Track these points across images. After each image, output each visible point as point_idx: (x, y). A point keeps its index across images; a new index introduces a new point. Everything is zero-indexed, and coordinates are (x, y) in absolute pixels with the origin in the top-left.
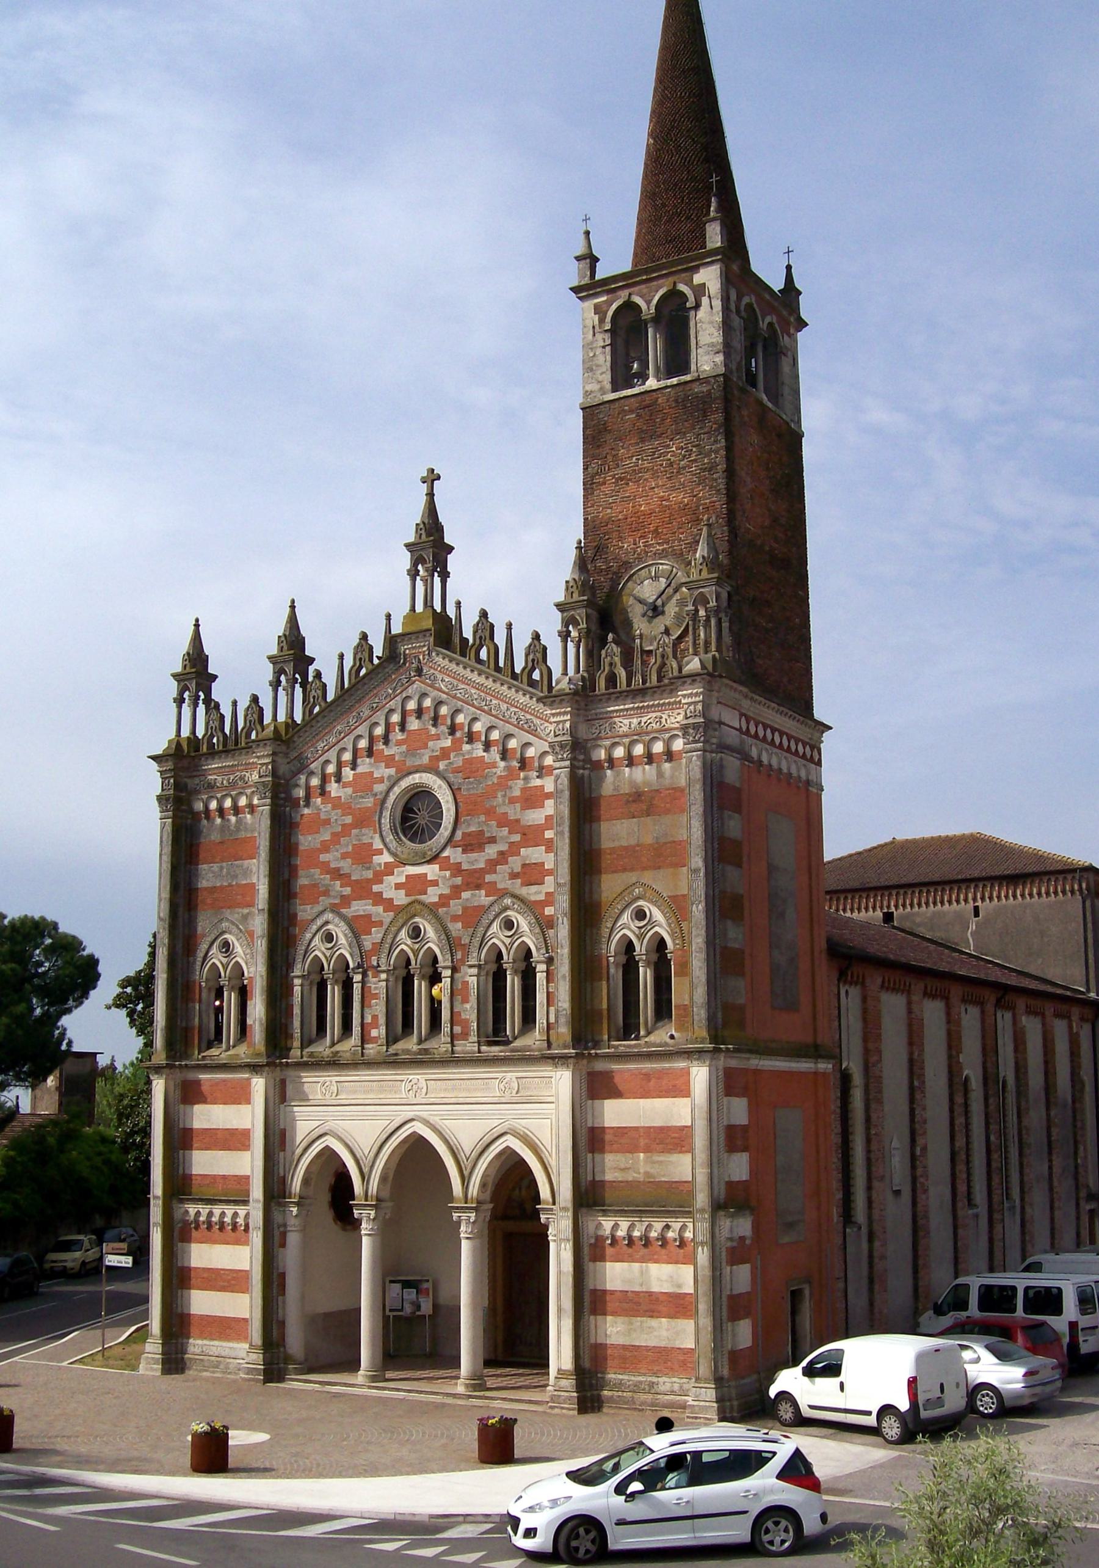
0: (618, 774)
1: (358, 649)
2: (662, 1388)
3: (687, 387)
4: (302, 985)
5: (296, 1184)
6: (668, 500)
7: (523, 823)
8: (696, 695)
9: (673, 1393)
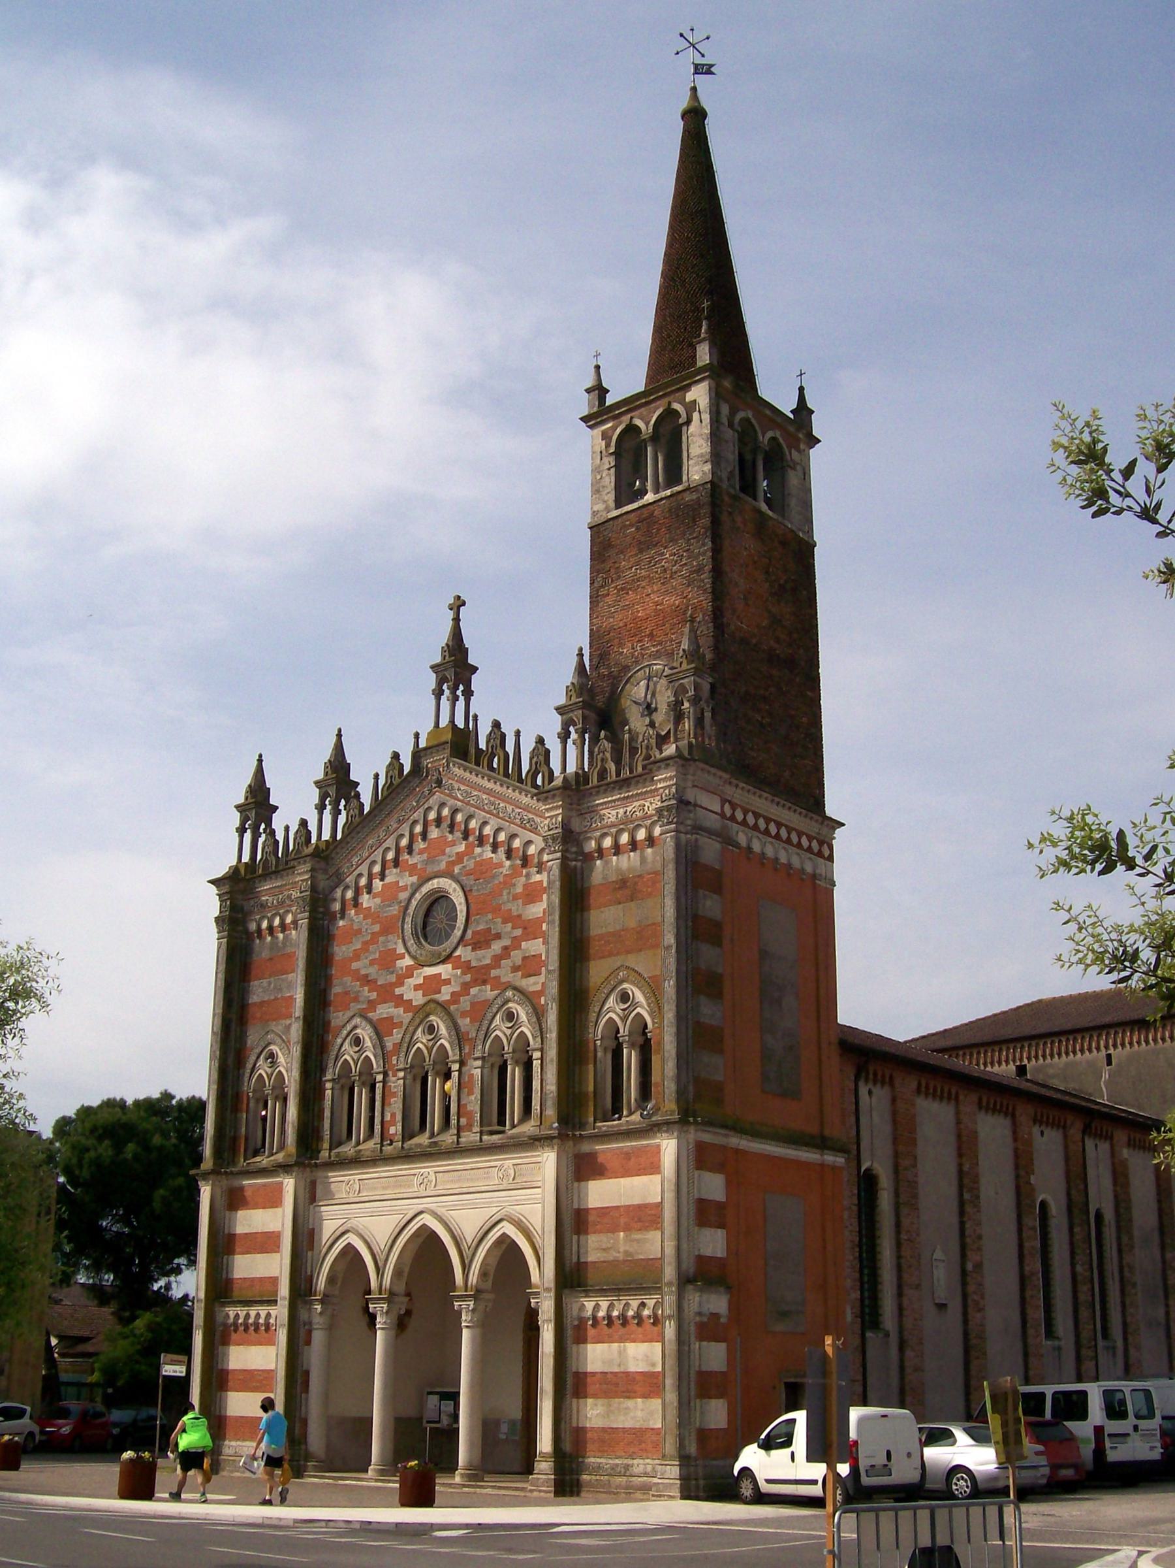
0: (607, 863)
1: (390, 767)
2: (636, 1470)
3: (680, 497)
4: (332, 1089)
5: (321, 1282)
7: (524, 917)
8: (671, 778)
9: (646, 1475)
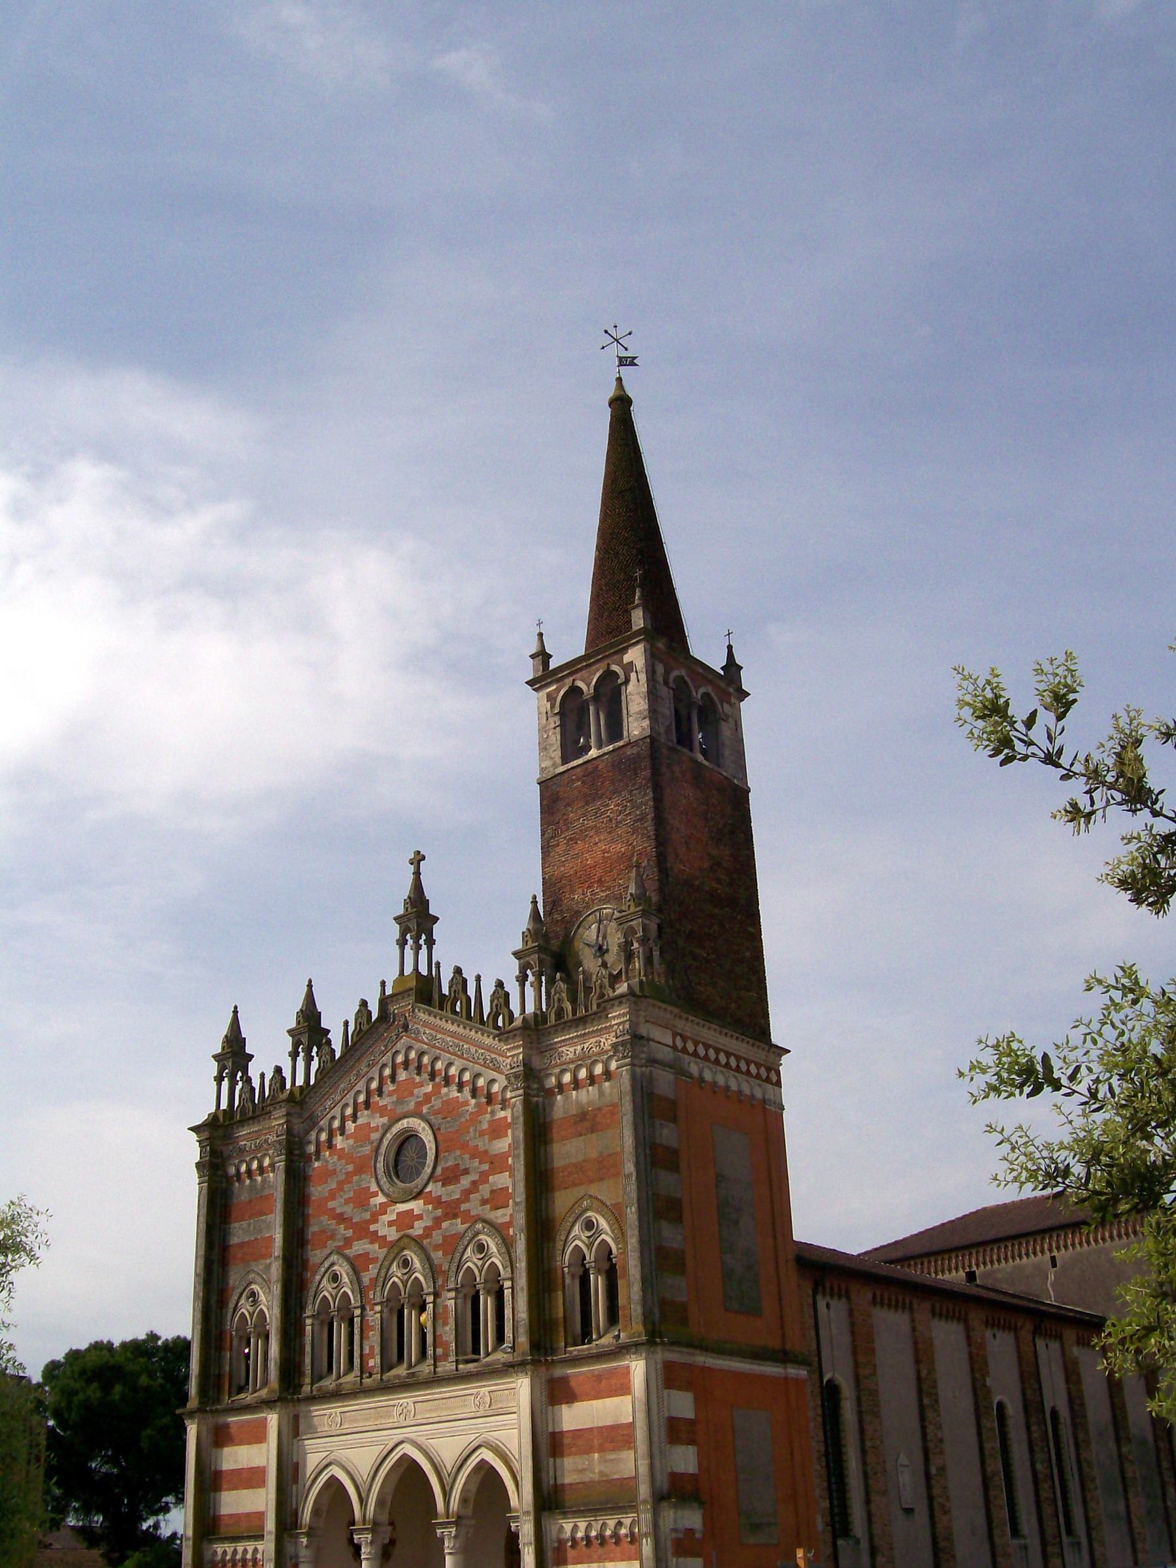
0: (566, 1098)
4: (312, 1325)
6: (609, 852)
8: (624, 1015)
